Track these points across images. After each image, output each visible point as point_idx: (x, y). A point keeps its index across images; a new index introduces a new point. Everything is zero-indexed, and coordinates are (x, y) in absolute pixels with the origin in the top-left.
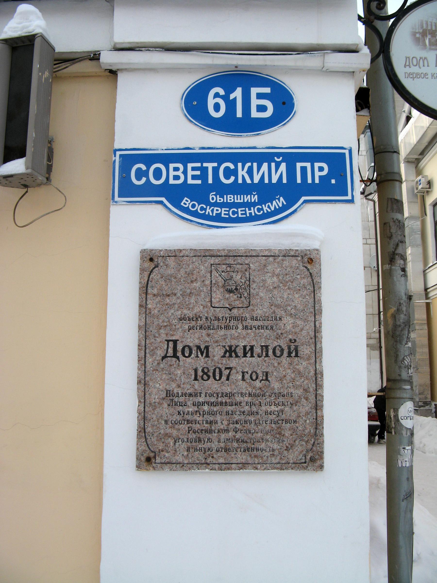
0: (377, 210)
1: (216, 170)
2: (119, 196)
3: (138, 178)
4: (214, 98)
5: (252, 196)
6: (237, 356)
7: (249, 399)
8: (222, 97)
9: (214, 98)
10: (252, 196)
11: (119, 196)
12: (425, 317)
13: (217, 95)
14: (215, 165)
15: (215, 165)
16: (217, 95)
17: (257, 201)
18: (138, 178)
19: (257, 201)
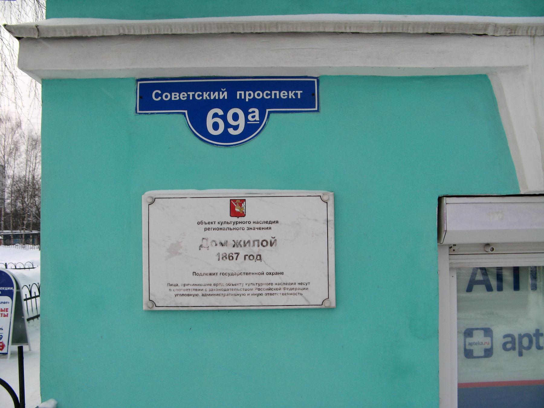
0: (264, 192)
1: (194, 95)
2: (140, 84)
3: (156, 97)
4: (213, 117)
5: (221, 93)
6: (241, 246)
7: (257, 286)
8: (220, 117)
9: (213, 117)
10: (221, 93)
11: (140, 84)
12: (522, 193)
13: (215, 115)
14: (194, 93)
15: (194, 93)
16: (215, 115)
17: (226, 98)
18: (156, 97)
19: (226, 98)
